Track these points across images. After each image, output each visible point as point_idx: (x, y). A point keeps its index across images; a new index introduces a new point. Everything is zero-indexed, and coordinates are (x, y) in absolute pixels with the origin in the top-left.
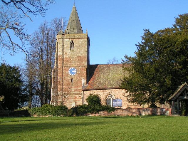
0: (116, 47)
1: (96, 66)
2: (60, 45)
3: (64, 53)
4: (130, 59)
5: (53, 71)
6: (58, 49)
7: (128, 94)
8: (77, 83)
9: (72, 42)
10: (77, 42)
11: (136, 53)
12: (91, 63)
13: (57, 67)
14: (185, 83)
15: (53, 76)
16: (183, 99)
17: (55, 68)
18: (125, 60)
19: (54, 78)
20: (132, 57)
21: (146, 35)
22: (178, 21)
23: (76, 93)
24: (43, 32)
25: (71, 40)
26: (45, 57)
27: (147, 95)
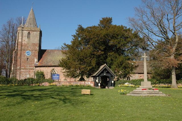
0: (59, 39)
1: (45, 51)
2: (20, 35)
3: (23, 40)
4: (68, 46)
5: (14, 52)
6: (18, 37)
7: (64, 71)
8: (31, 61)
9: (29, 33)
10: (32, 33)
11: (72, 42)
12: (42, 48)
13: (17, 50)
14: (105, 64)
15: (14, 56)
16: (104, 75)
17: (16, 50)
18: (64, 46)
19: (15, 57)
20: (69, 44)
21: (79, 29)
22: (102, 22)
23: (30, 68)
24: (10, 25)
25: (28, 32)
26: (10, 43)
27: (78, 72)
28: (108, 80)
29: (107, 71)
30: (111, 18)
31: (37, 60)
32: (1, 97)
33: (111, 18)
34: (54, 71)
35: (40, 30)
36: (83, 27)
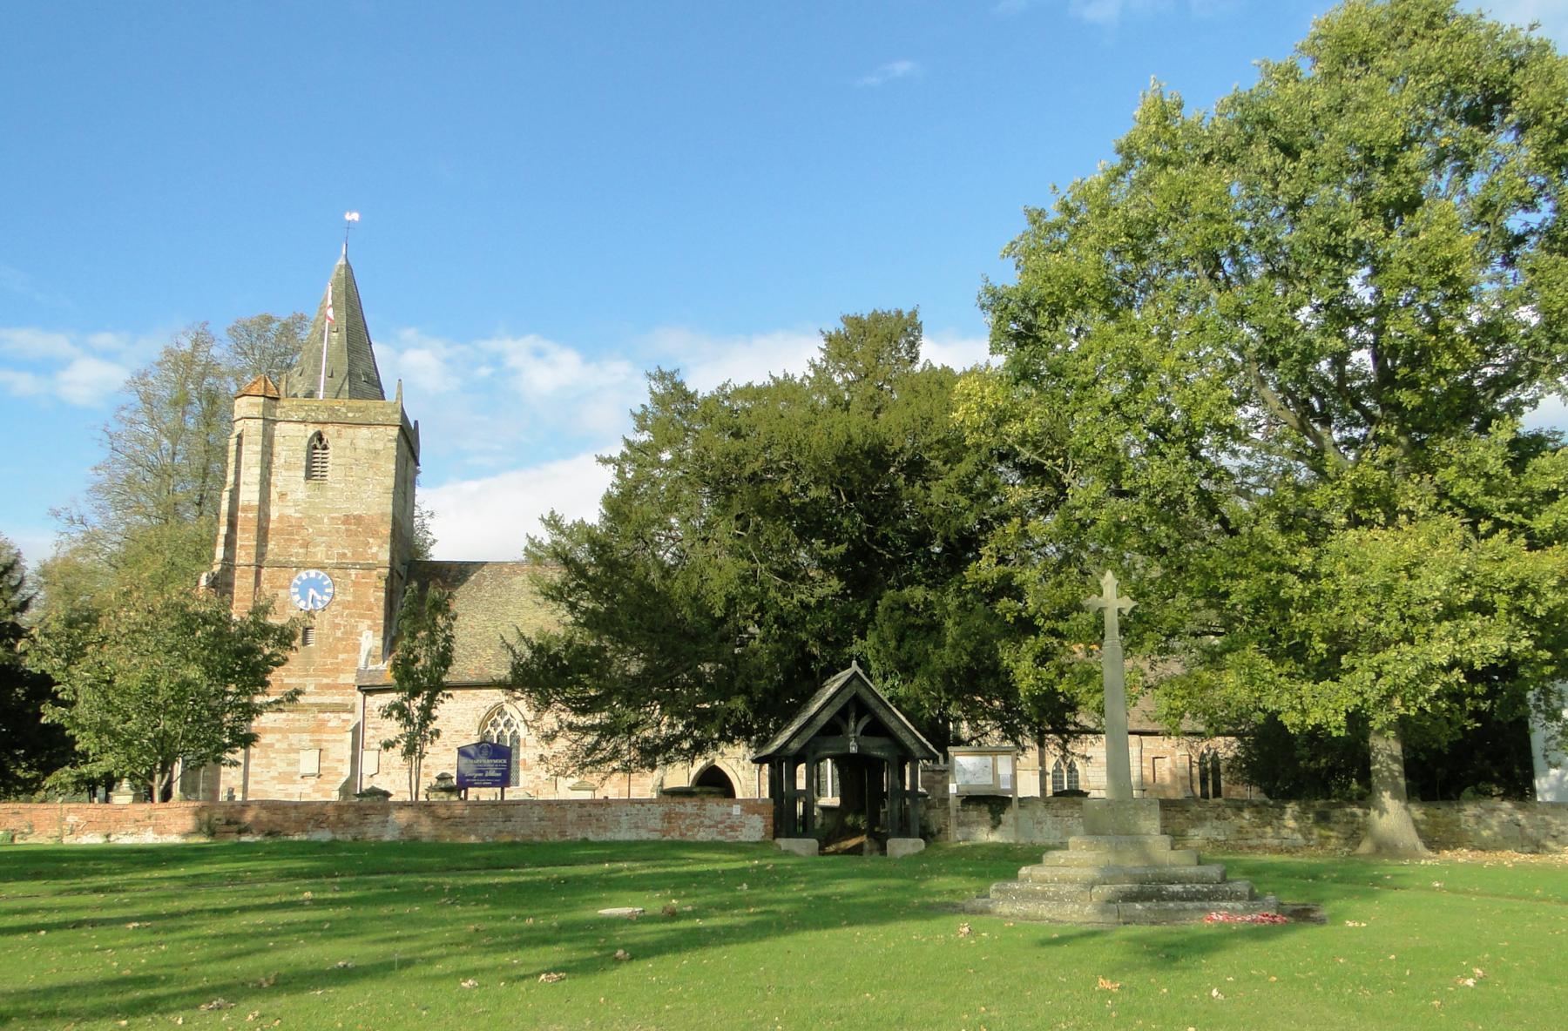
3: (274, 496)
6: (237, 473)
8: (333, 651)
22: (839, 348)
23: (327, 699)
25: (311, 430)
28: (801, 784)
29: (865, 721)
30: (914, 314)
31: (379, 643)
32: (16, 892)
33: (914, 314)
34: (508, 724)
35: (404, 417)
36: (691, 389)
